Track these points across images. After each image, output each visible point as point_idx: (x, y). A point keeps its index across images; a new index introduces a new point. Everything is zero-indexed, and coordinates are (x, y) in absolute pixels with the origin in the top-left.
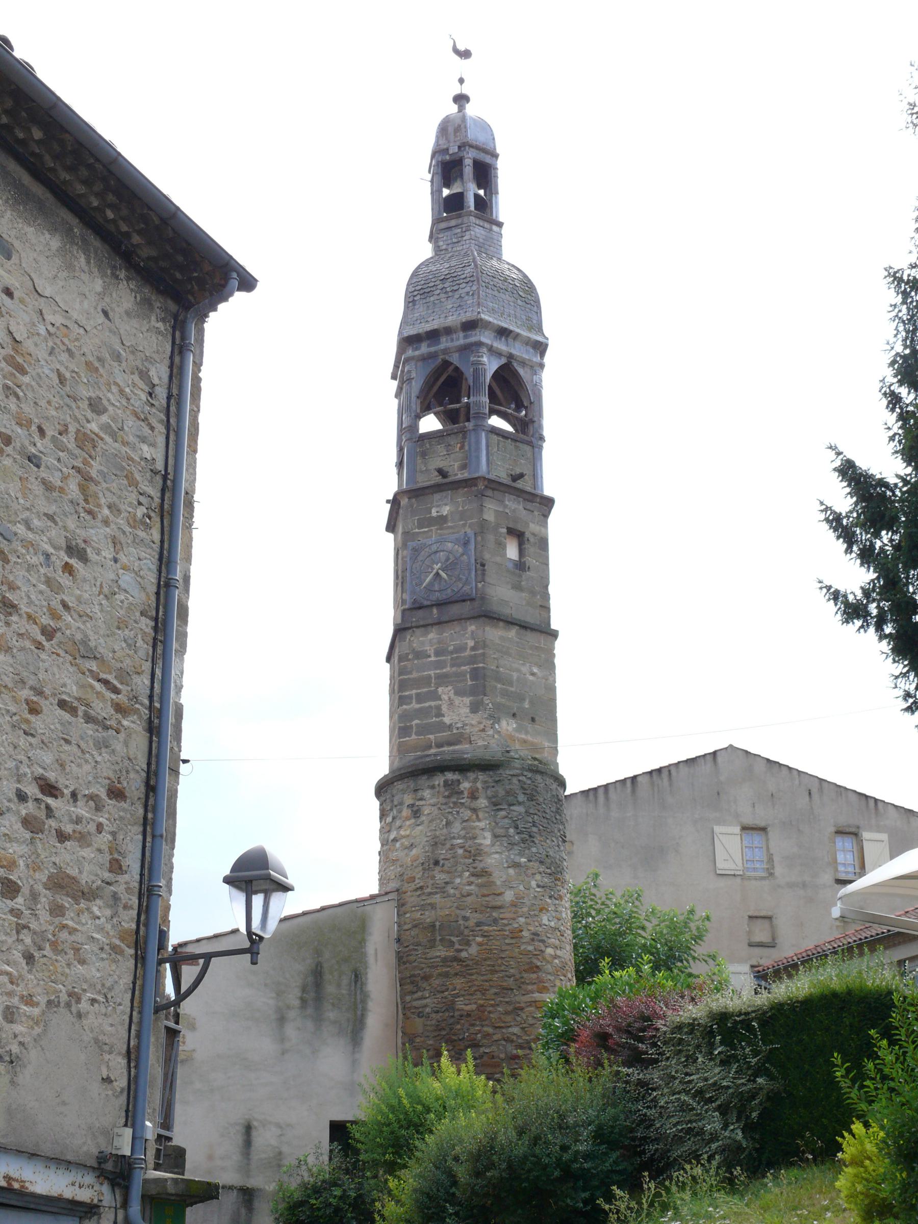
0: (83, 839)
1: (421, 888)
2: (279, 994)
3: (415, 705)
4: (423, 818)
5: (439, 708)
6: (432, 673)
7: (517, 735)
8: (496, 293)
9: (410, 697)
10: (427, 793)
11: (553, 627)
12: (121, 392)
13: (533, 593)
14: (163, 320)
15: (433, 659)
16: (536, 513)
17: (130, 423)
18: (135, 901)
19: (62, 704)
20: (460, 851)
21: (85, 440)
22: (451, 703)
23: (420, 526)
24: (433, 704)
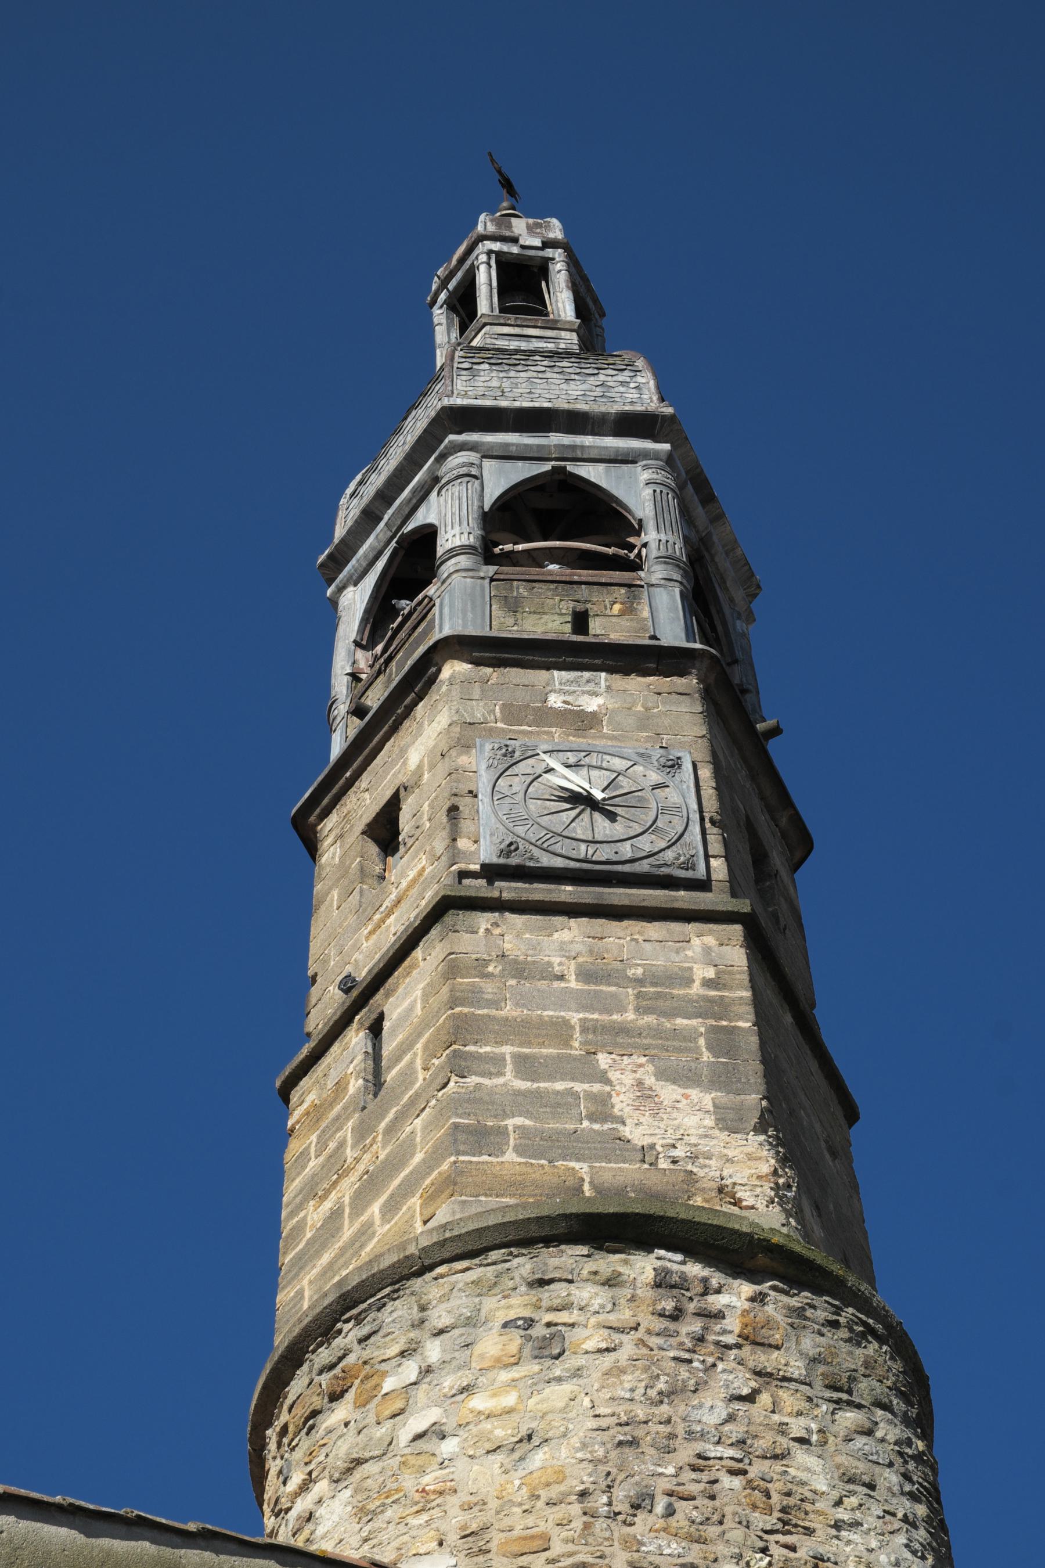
6: (575, 1017)
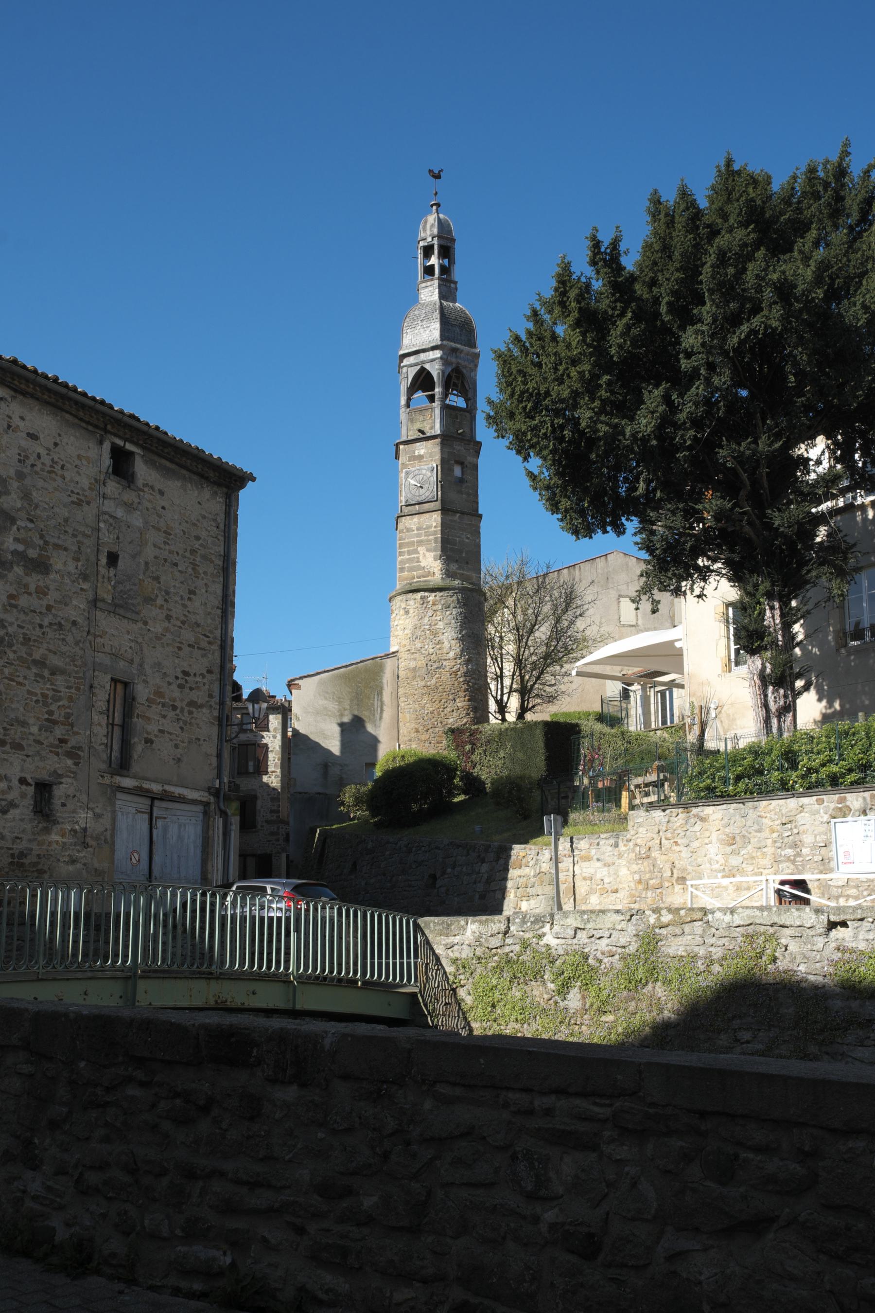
0: (198, 688)
1: (409, 650)
2: (340, 702)
3: (407, 557)
4: (410, 615)
5: (418, 558)
7: (458, 571)
8: (450, 327)
9: (404, 552)
10: (412, 602)
11: (480, 512)
12: (206, 530)
13: (468, 494)
14: (222, 497)
15: (416, 532)
16: (471, 451)
17: (210, 540)
18: (218, 707)
19: (189, 645)
20: (428, 632)
21: (193, 552)
22: (424, 555)
23: (410, 461)
24: (415, 556)
